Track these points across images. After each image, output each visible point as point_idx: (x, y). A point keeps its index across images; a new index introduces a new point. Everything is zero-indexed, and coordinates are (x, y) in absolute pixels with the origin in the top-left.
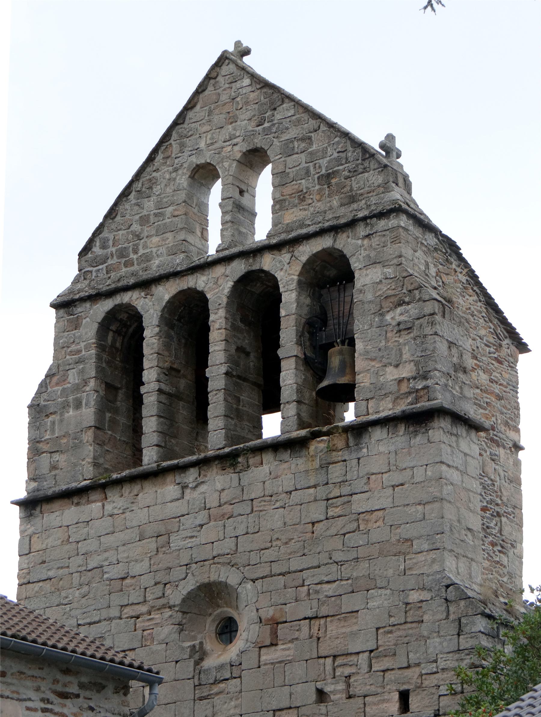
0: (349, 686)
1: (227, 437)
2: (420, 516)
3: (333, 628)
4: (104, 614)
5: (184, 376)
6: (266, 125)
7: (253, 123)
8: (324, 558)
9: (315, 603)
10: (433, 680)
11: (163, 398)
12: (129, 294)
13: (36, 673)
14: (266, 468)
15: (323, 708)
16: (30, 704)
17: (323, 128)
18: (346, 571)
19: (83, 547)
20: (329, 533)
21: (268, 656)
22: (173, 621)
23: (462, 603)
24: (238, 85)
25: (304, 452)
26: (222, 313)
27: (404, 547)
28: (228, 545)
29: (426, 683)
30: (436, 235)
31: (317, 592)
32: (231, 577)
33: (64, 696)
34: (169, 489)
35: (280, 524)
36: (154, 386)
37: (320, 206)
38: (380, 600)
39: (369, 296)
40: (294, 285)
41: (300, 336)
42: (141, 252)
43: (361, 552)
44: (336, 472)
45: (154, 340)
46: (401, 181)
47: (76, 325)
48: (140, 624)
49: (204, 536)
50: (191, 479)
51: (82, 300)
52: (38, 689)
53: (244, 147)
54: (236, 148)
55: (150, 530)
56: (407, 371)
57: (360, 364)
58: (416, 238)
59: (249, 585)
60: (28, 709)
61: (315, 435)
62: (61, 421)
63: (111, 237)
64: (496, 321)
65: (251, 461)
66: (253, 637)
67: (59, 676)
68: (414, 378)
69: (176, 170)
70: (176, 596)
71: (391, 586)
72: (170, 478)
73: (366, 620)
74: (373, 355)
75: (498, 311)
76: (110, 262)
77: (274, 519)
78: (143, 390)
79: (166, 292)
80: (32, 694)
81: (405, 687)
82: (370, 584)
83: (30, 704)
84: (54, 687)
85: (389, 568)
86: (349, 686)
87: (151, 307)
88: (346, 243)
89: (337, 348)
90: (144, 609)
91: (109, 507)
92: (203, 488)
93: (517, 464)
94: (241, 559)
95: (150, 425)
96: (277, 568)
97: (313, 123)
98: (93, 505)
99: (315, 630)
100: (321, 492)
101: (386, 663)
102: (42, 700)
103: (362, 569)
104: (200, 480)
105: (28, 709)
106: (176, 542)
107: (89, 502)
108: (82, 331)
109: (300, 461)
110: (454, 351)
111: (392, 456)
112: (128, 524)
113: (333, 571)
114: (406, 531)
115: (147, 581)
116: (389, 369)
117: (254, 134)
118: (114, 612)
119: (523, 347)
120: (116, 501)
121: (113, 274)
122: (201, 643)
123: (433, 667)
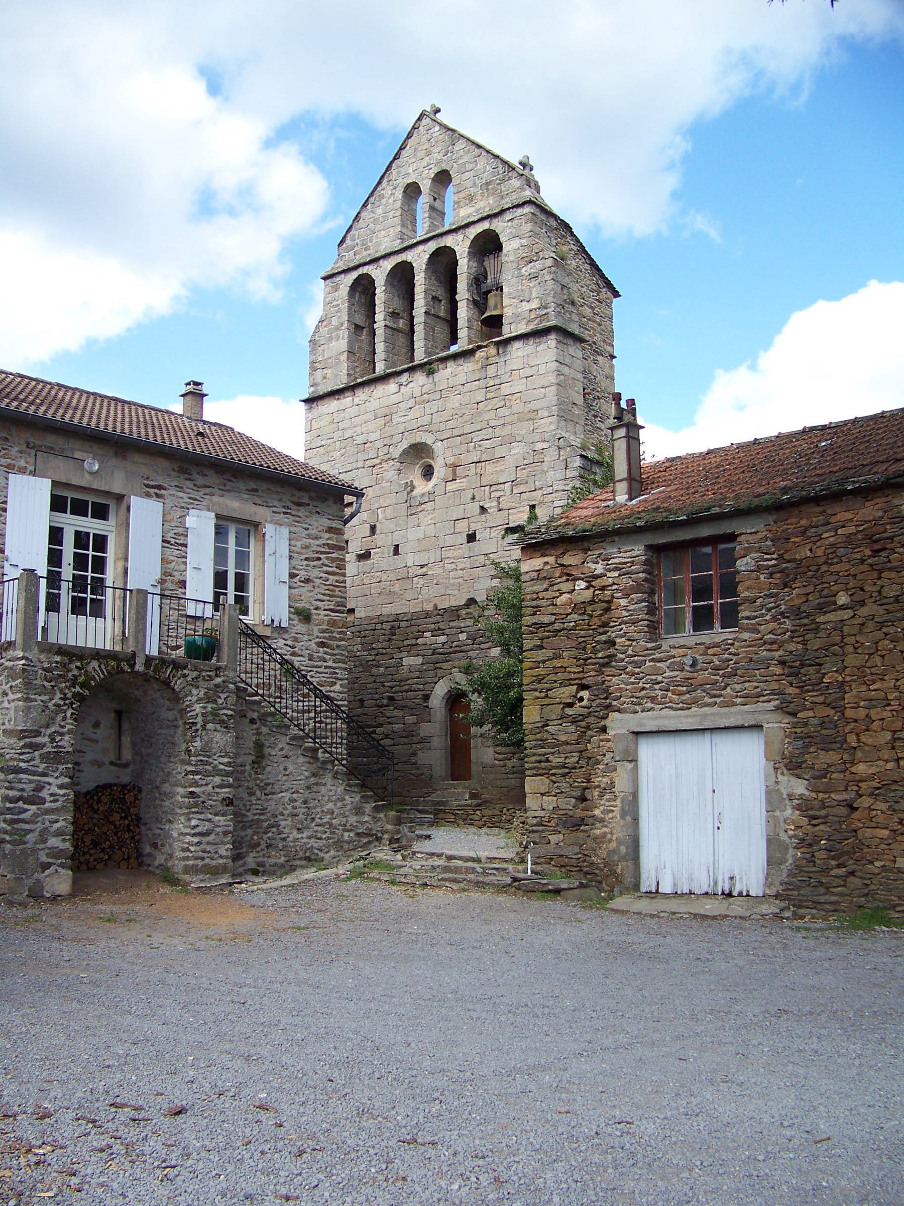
0: (499, 503)
1: (426, 352)
2: (542, 396)
3: (490, 468)
4: (355, 465)
5: (402, 318)
6: (449, 155)
7: (442, 154)
8: (484, 425)
9: (479, 453)
10: (550, 498)
11: (389, 331)
12: (367, 267)
13: (279, 490)
14: (449, 370)
15: (483, 517)
16: (275, 509)
17: (484, 153)
18: (498, 432)
19: (341, 425)
20: (487, 409)
21: (451, 486)
22: (394, 468)
23: (568, 449)
24: (432, 131)
25: (472, 359)
26: (422, 275)
27: (533, 416)
28: (426, 420)
29: (546, 500)
30: (556, 220)
31: (480, 446)
32: (428, 439)
33: (300, 504)
34: (391, 386)
35: (457, 405)
36: (382, 323)
37: (481, 204)
38: (518, 449)
39: (512, 258)
40: (466, 254)
41: (470, 286)
42: (375, 241)
43: (507, 420)
44: (491, 370)
45: (382, 295)
46: (532, 185)
47: (336, 289)
48: (375, 470)
49: (412, 415)
50: (404, 379)
51: (339, 273)
52: (280, 500)
53: (436, 170)
54: (431, 171)
55: (381, 413)
56: (535, 304)
57: (506, 301)
58: (542, 221)
59: (439, 444)
60: (274, 512)
61: (479, 347)
62: (328, 348)
63: (357, 233)
64: (597, 276)
65: (440, 366)
66: (442, 475)
67: (295, 492)
68: (539, 308)
69: (395, 188)
70: (396, 453)
71: (525, 440)
72: (392, 380)
73: (510, 462)
74: (514, 295)
75: (599, 270)
76: (356, 249)
77: (454, 402)
78: (375, 326)
79: (388, 265)
80: (276, 503)
81: (533, 503)
82: (511, 440)
83: (275, 509)
84: (292, 499)
85: (522, 429)
86: (499, 503)
87: (380, 274)
88: (498, 225)
89: (493, 293)
90: (377, 461)
91: (356, 400)
92: (411, 385)
93: (612, 367)
94: (434, 428)
95: (380, 347)
96: (456, 432)
97: (477, 151)
98: (347, 399)
99: (478, 470)
100: (482, 383)
101: (522, 488)
102: (284, 507)
103: (507, 430)
104: (410, 380)
105: (274, 512)
106: (396, 419)
107: (344, 398)
108: (340, 292)
109: (469, 365)
110: (565, 291)
111: (526, 358)
112: (368, 410)
113: (489, 433)
114: (534, 405)
115: (379, 444)
116: (524, 303)
117: (441, 161)
118: (360, 464)
119: (616, 294)
120: (361, 395)
121: (357, 257)
122: (412, 481)
123: (550, 490)
